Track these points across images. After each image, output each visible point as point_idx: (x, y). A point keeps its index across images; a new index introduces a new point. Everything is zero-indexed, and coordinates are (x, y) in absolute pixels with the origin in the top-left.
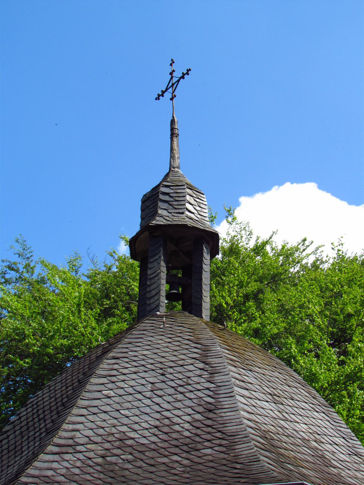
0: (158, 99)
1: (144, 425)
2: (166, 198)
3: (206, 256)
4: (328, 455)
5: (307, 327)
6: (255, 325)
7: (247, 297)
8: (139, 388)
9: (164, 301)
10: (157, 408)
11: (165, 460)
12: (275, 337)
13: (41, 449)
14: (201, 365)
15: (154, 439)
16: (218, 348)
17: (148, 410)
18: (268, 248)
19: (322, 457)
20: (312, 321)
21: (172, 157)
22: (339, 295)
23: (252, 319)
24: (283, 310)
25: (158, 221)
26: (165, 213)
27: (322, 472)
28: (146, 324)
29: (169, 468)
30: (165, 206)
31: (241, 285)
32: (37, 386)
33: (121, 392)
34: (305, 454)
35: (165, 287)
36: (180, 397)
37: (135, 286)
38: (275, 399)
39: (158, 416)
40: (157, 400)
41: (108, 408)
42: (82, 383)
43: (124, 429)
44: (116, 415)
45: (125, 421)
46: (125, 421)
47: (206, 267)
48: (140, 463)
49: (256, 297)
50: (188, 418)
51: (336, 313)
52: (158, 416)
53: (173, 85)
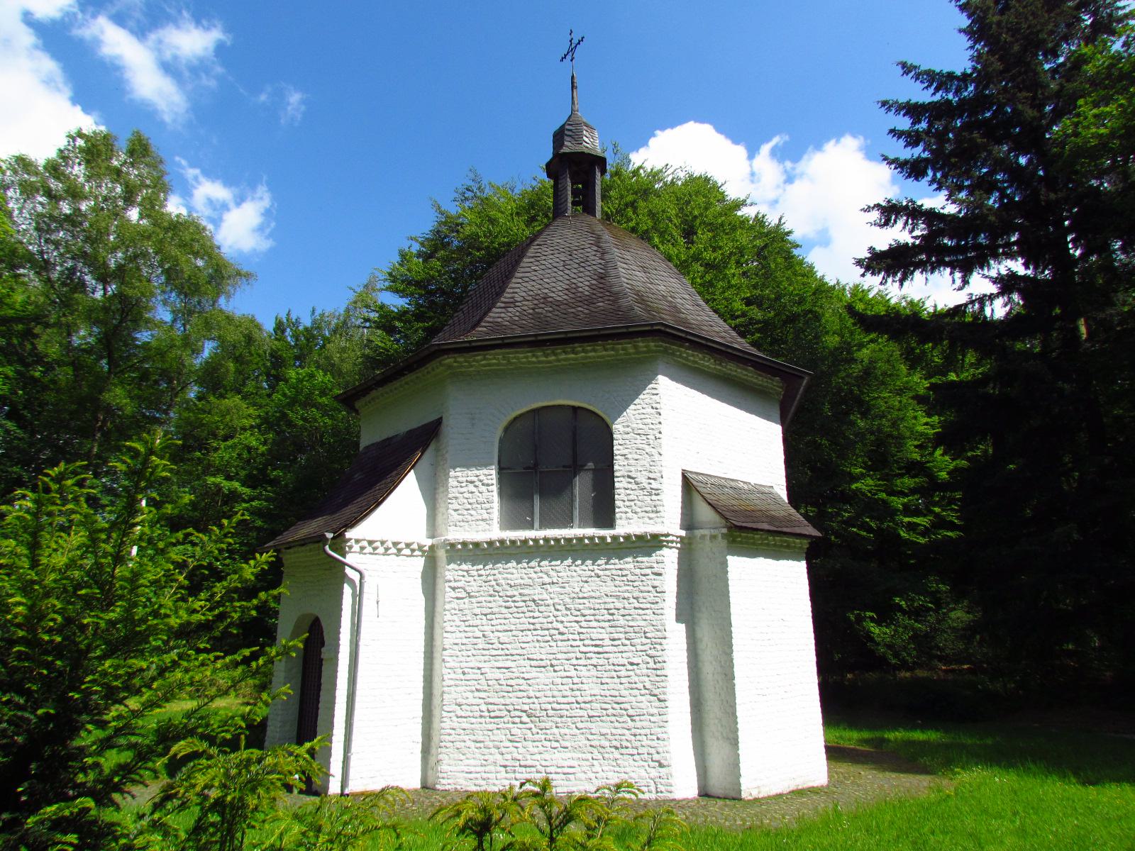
0: (562, 60)
1: (560, 288)
2: (570, 133)
3: (598, 174)
4: (679, 306)
5: (667, 225)
6: (632, 224)
7: (627, 205)
8: (555, 265)
9: (570, 205)
10: (567, 277)
11: (573, 310)
12: (646, 232)
13: (493, 305)
14: (596, 248)
15: (566, 297)
16: (606, 236)
17: (561, 279)
18: (641, 171)
19: (675, 307)
20: (671, 221)
21: (573, 103)
22: (688, 203)
23: (630, 220)
24: (652, 214)
25: (565, 150)
26: (569, 144)
27: (675, 316)
28: (558, 222)
29: (576, 315)
30: (568, 139)
31: (622, 197)
32: (490, 265)
33: (543, 267)
34: (664, 305)
35: (570, 199)
36: (582, 269)
37: (550, 202)
38: (644, 269)
39: (568, 282)
40: (567, 272)
41: (535, 278)
42: (517, 263)
43: (546, 291)
44: (541, 282)
45: (547, 286)
46: (547, 286)
47: (598, 182)
48: (557, 313)
49: (633, 205)
50: (587, 283)
51: (687, 216)
52: (568, 282)
53: (572, 50)
